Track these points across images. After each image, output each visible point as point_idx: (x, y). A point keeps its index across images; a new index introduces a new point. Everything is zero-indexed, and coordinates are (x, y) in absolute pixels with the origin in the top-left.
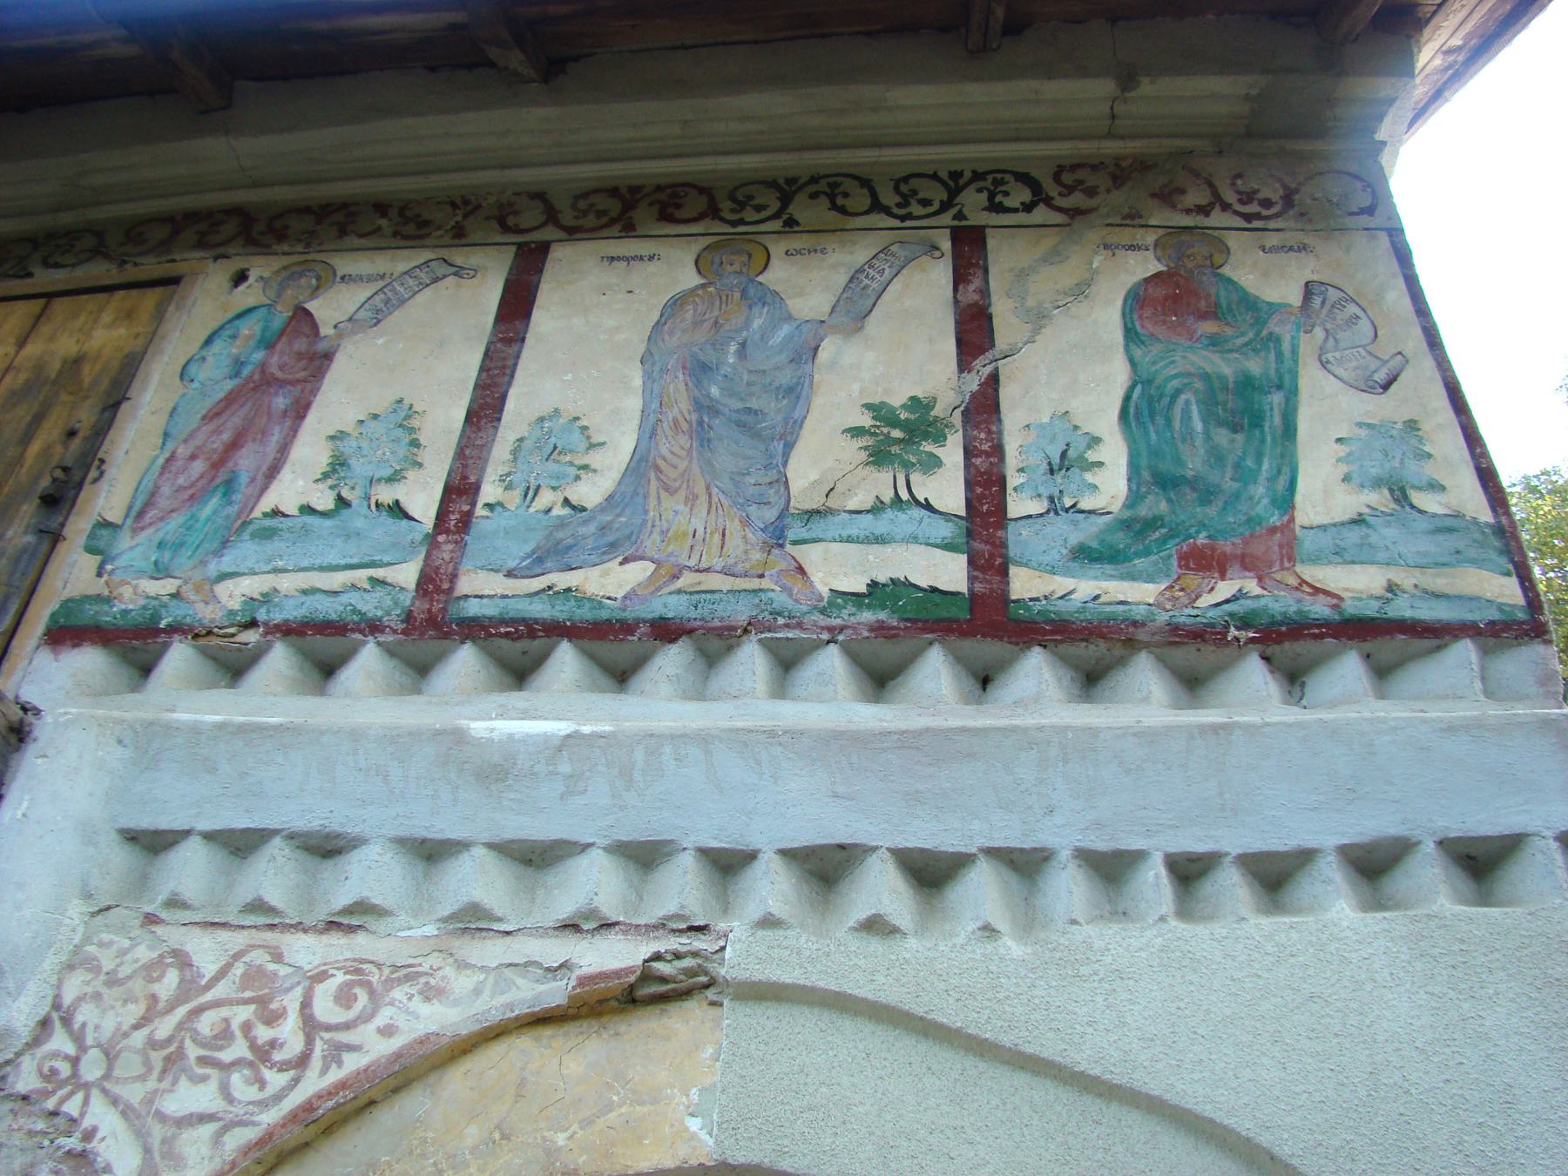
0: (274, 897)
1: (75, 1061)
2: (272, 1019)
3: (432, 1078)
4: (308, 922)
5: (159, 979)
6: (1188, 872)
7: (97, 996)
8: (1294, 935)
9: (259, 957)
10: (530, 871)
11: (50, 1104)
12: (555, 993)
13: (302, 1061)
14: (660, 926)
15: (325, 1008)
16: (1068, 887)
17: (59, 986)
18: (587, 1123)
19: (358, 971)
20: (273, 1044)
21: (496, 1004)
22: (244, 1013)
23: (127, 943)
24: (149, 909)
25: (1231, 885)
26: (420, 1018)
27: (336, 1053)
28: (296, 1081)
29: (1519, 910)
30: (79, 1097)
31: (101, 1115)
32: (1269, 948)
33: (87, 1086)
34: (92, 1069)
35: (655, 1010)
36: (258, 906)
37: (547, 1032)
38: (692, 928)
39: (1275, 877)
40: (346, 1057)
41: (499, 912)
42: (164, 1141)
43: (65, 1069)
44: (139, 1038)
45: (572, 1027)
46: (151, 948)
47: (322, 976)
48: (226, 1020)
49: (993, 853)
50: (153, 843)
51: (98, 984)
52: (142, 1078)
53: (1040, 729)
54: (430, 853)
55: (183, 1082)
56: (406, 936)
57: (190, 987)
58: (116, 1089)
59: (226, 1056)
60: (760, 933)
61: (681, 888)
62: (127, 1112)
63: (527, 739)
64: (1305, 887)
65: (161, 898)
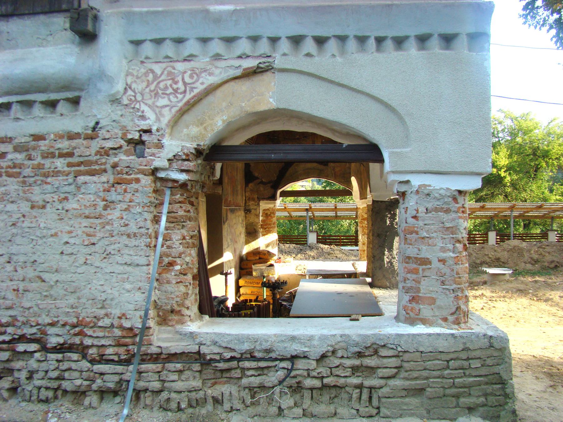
0: (170, 55)
1: (135, 97)
2: (176, 83)
3: (214, 92)
4: (180, 59)
5: (148, 76)
6: (380, 40)
7: (135, 82)
8: (401, 57)
9: (170, 69)
10: (229, 43)
11: (132, 106)
12: (239, 72)
13: (185, 92)
14: (260, 56)
15: (187, 80)
16: (352, 44)
17: (126, 80)
18: (249, 101)
19: (193, 70)
20: (178, 88)
21: (225, 76)
22: (169, 82)
23: (138, 68)
24: (141, 60)
25: (389, 44)
26: (210, 80)
27: (192, 89)
28: (184, 96)
29: (453, 52)
30: (138, 104)
31: (144, 107)
32: (396, 60)
33: (139, 102)
34: (139, 98)
35: (260, 75)
36: (167, 57)
37: (237, 81)
38: (267, 56)
39: (399, 42)
40: (194, 90)
41: (223, 55)
42: (159, 112)
43: (133, 98)
44: (147, 90)
45: (242, 80)
46: (144, 69)
47: (185, 72)
48: (166, 84)
49: (335, 36)
50: (137, 43)
51: (135, 79)
52: (151, 99)
53: (347, 5)
54: (205, 41)
55: (160, 99)
56: (203, 61)
57: (156, 77)
58: (146, 102)
59: (168, 92)
60: (283, 57)
61: (264, 47)
62: (149, 106)
63: (224, 12)
64: (406, 44)
65: (143, 57)
